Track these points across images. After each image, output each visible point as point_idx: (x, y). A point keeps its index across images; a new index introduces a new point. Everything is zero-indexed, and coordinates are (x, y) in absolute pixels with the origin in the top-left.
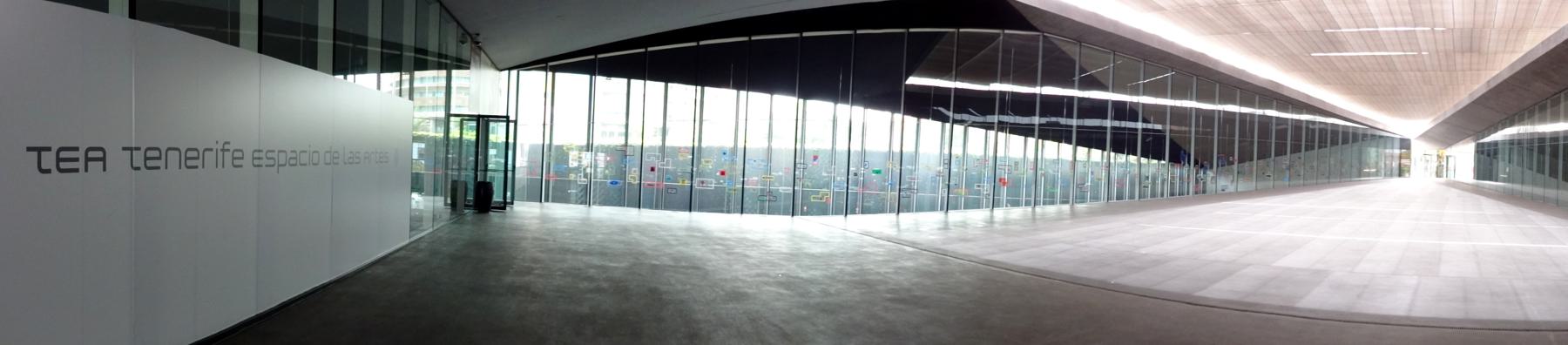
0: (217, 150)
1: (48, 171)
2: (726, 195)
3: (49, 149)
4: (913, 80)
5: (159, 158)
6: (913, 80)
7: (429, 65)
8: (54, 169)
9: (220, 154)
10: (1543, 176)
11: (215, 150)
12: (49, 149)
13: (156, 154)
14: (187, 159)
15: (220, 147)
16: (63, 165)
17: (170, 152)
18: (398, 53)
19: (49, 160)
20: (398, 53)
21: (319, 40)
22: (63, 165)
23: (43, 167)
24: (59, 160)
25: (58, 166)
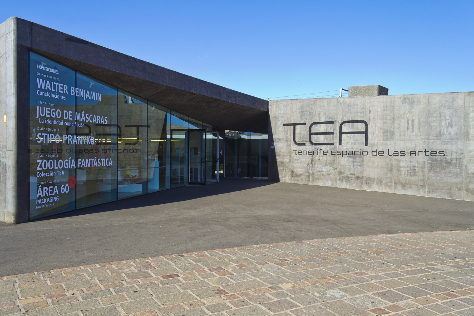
0: (318, 151)
1: (297, 154)
2: (441, 169)
3: (297, 151)
4: (111, 139)
5: (301, 153)
6: (111, 139)
7: (140, 139)
8: (392, 155)
9: (319, 152)
10: (159, 137)
11: (317, 151)
12: (297, 151)
13: (301, 152)
14: (308, 153)
15: (319, 150)
16: (299, 153)
17: (304, 152)
18: (266, 137)
19: (297, 152)
20: (266, 137)
21: (31, 146)
22: (299, 153)
23: (296, 154)
24: (298, 153)
25: (298, 154)
